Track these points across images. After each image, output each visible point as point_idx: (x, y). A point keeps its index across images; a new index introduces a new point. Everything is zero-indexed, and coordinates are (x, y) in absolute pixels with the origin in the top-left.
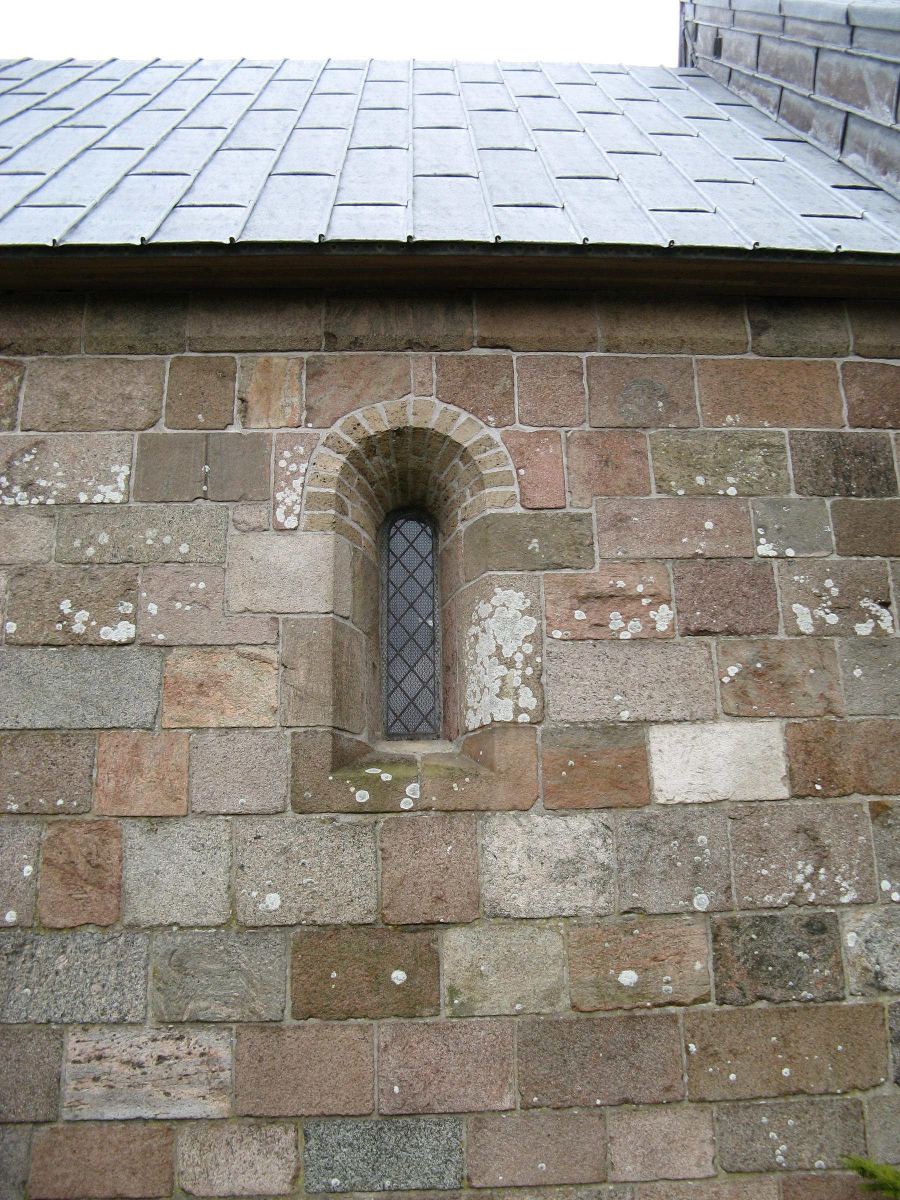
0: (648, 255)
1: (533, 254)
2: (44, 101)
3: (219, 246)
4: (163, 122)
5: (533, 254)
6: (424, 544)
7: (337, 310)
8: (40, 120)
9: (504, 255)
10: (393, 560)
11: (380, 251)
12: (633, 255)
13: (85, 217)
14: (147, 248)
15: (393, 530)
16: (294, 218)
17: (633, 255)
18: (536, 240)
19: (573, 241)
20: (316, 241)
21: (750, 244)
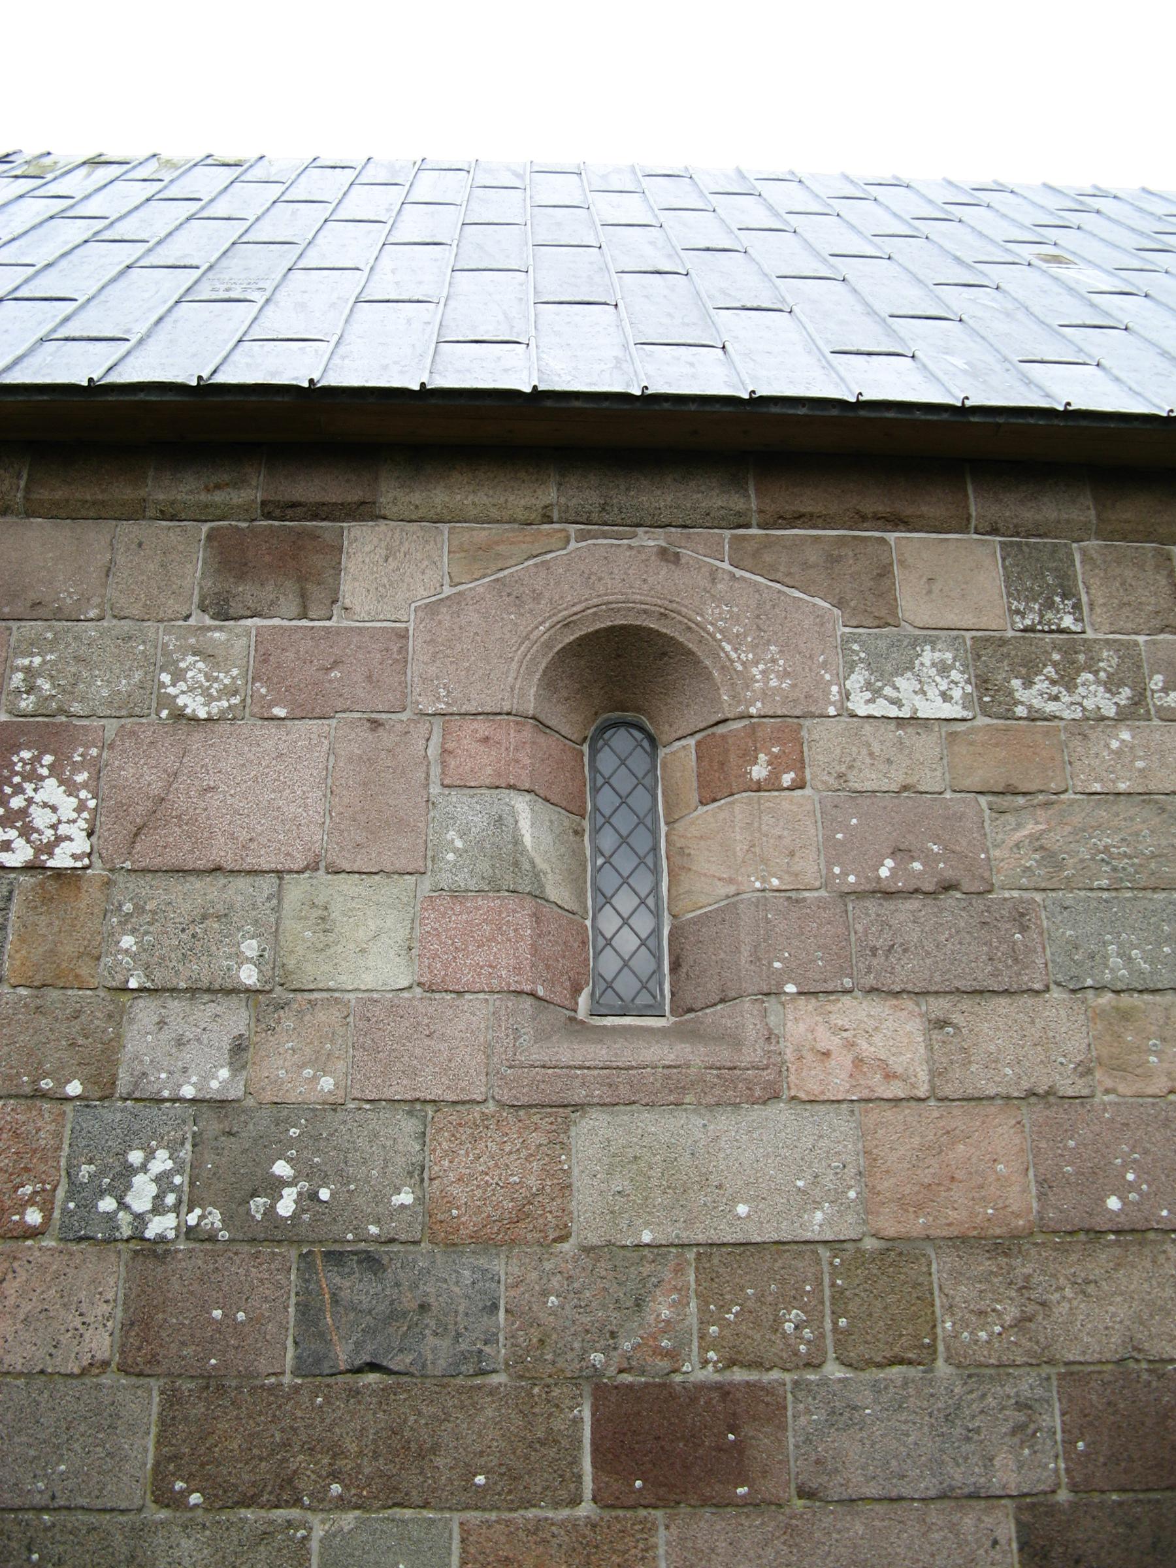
0: (835, 412)
1: (657, 407)
2: (72, 206)
3: (517, 394)
4: (74, 231)
5: (657, 407)
6: (639, 762)
7: (151, 473)
8: (74, 231)
9: (110, 399)
10: (600, 781)
11: (577, 404)
12: (693, 407)
13: (128, 353)
14: (207, 391)
15: (601, 742)
16: (178, 356)
17: (918, 415)
18: (345, 384)
19: (845, 398)
20: (85, 383)
21: (1060, 403)
